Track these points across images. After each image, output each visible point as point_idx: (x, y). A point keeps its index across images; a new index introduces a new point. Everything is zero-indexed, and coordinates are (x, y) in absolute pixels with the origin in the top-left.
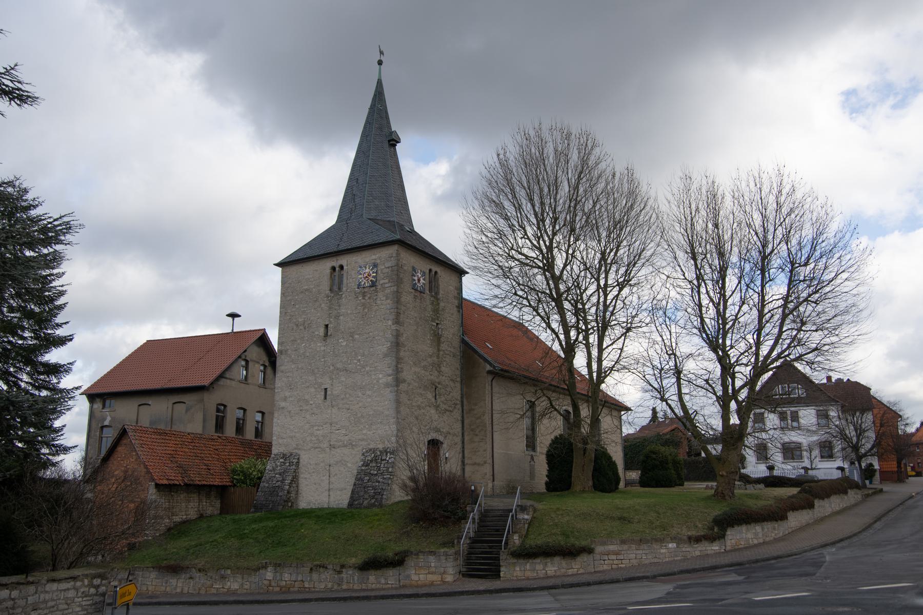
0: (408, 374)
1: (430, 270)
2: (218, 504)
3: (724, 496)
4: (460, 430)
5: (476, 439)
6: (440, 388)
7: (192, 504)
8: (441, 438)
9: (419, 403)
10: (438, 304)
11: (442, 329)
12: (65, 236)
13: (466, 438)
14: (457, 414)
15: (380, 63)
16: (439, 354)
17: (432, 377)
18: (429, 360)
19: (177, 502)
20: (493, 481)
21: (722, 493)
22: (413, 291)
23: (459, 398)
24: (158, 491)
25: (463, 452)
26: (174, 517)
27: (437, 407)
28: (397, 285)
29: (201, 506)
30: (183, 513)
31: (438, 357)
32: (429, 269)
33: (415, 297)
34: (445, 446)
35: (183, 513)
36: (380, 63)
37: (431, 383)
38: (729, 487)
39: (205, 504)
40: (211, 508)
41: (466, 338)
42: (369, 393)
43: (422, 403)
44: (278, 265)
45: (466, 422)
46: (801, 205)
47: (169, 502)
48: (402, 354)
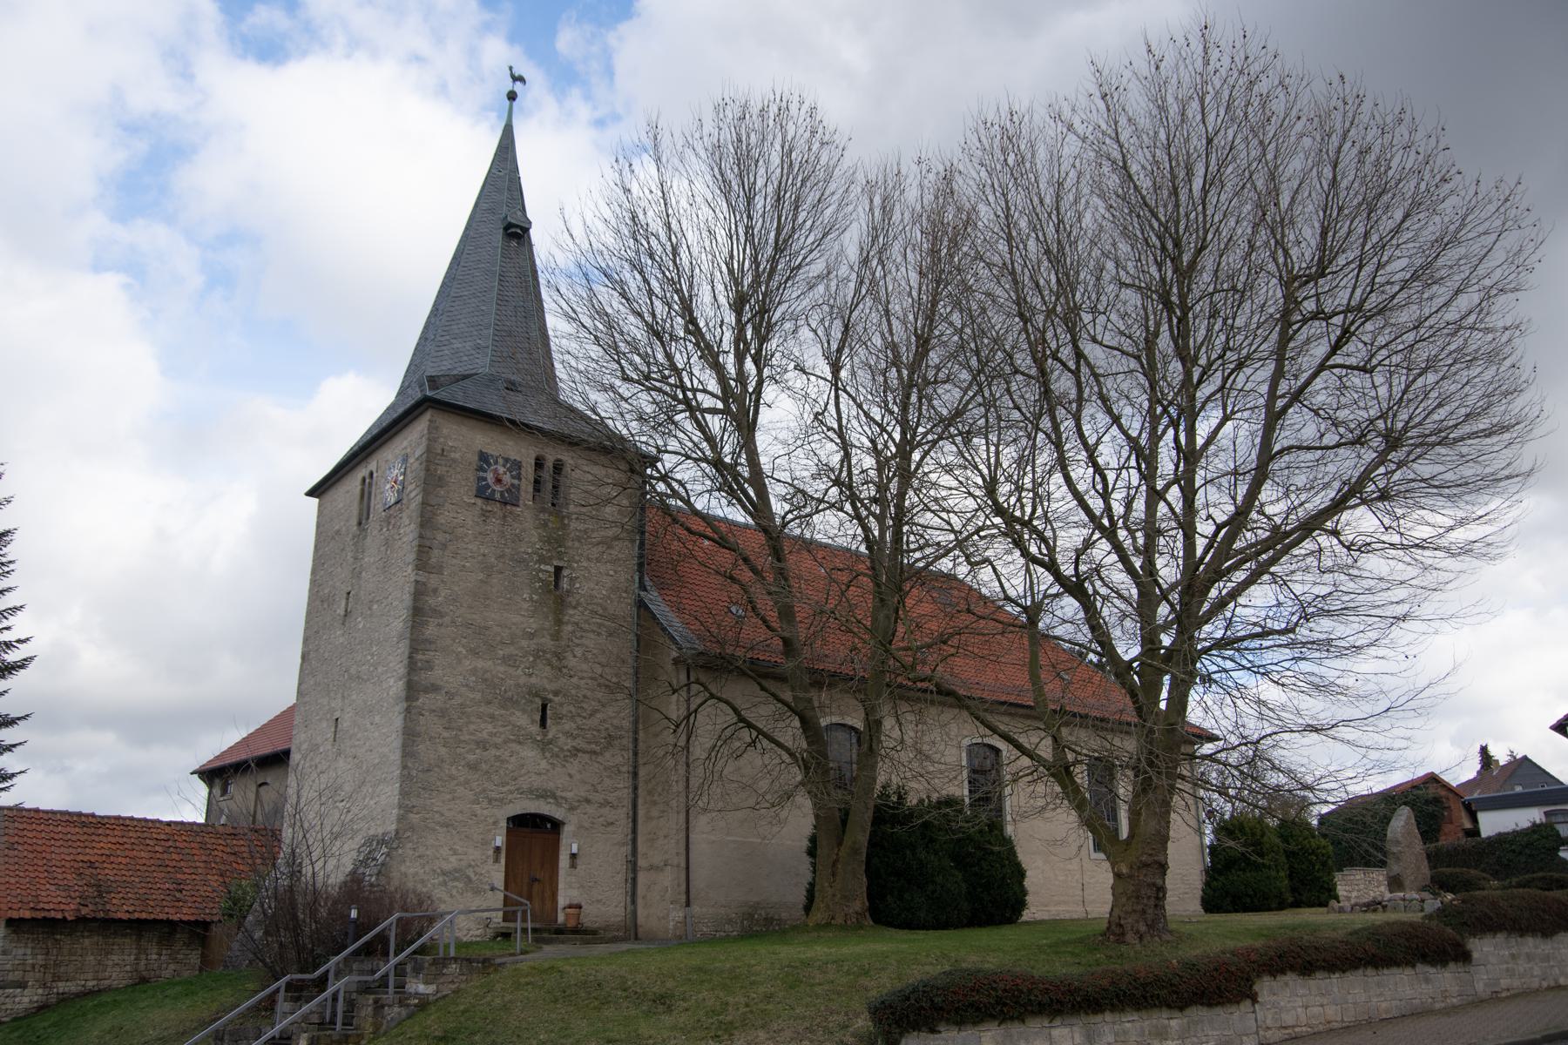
0: (447, 672)
1: (539, 463)
2: (195, 958)
3: (1123, 934)
4: (626, 794)
5: (655, 813)
6: (561, 705)
7: (115, 957)
8: (558, 813)
9: (485, 735)
10: (564, 527)
11: (572, 579)
12: (1034, 612)
13: (641, 813)
14: (618, 757)
15: (512, 96)
16: (558, 632)
17: (533, 680)
18: (524, 643)
19: (70, 954)
20: (688, 904)
21: (1121, 926)
22: (479, 502)
23: (627, 724)
24: (15, 932)
25: (634, 841)
26: (60, 984)
27: (544, 746)
28: (902, 552)
29: (143, 963)
30: (90, 976)
31: (556, 636)
32: (534, 456)
33: (485, 515)
34: (567, 830)
35: (90, 976)
36: (512, 96)
37: (530, 693)
38: (1140, 907)
39: (155, 957)
40: (172, 967)
41: (654, 599)
42: (377, 719)
43: (491, 734)
44: (311, 493)
45: (642, 772)
46: (1304, 83)
47: (47, 954)
48: (431, 630)
